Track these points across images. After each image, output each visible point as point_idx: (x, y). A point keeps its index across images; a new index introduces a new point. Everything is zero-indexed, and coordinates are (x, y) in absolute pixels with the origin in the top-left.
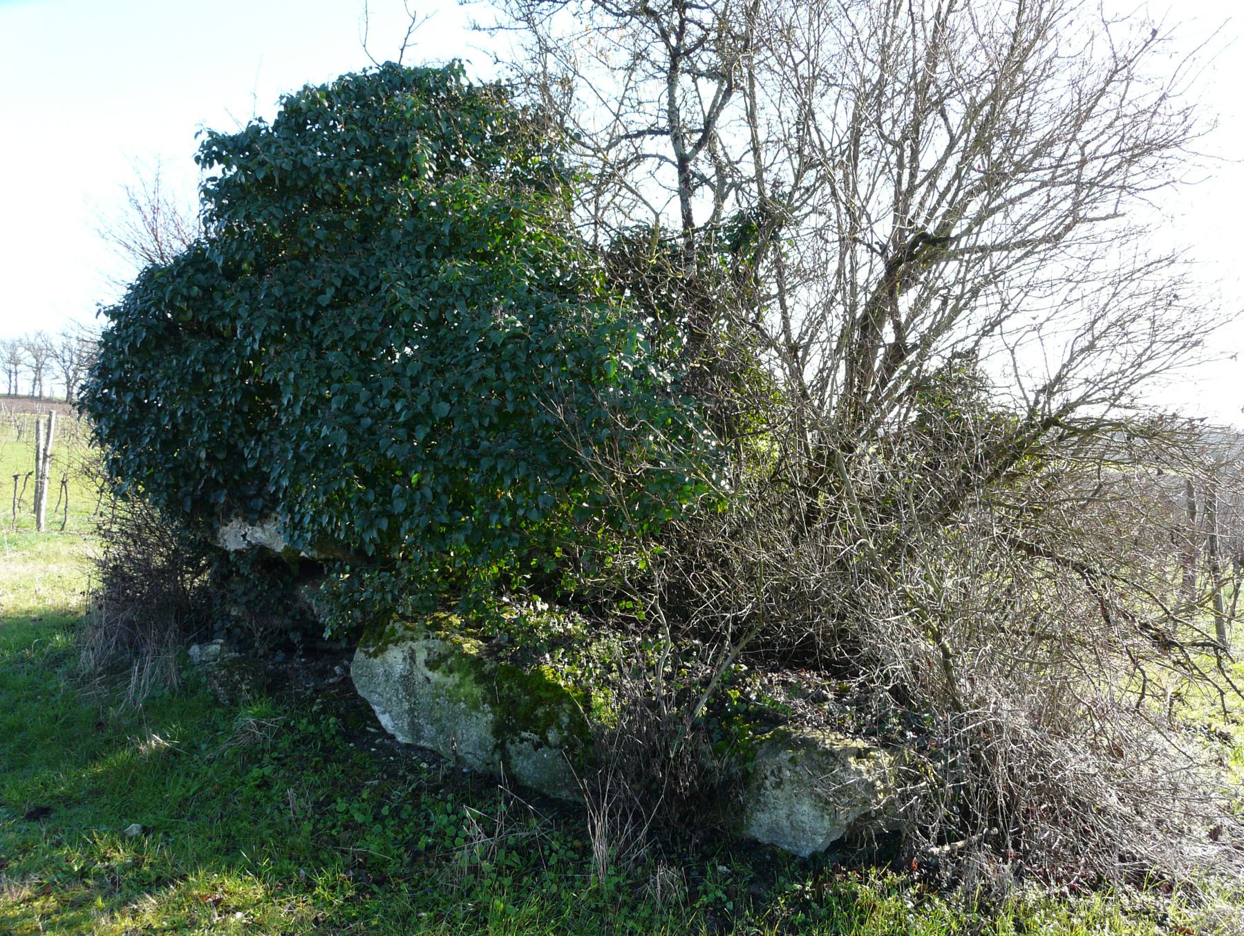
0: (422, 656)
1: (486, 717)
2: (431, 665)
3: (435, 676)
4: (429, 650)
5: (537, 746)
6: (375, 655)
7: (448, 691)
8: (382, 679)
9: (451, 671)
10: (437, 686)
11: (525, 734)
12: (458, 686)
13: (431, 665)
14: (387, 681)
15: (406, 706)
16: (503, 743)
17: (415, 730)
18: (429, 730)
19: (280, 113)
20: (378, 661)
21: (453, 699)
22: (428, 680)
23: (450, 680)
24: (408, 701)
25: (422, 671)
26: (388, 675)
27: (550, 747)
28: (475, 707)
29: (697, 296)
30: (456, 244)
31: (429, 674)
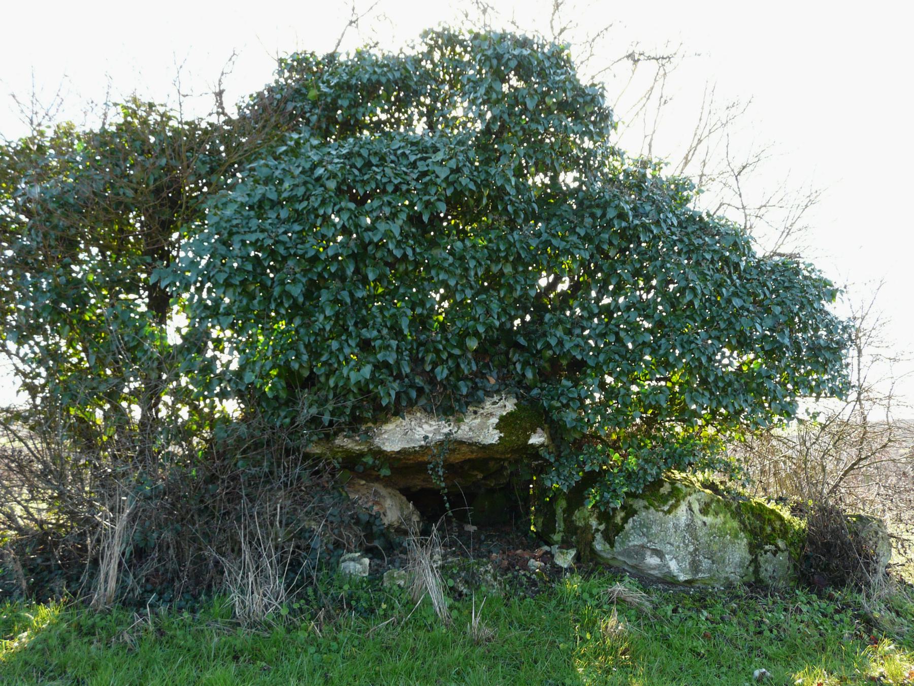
0: (696, 507)
1: (743, 541)
2: (704, 511)
3: (709, 519)
4: (698, 500)
5: (775, 554)
6: (669, 512)
7: (719, 529)
8: (672, 530)
9: (717, 514)
10: (712, 526)
11: (767, 547)
12: (725, 523)
13: (704, 511)
14: (675, 532)
15: (691, 548)
16: (756, 557)
17: (695, 567)
18: (706, 564)
19: (227, 399)
20: (671, 516)
21: (722, 533)
22: (705, 523)
23: (719, 520)
24: (693, 544)
25: (700, 518)
26: (676, 527)
27: (782, 551)
28: (736, 536)
29: (192, 516)
30: (424, 328)
31: (705, 518)
